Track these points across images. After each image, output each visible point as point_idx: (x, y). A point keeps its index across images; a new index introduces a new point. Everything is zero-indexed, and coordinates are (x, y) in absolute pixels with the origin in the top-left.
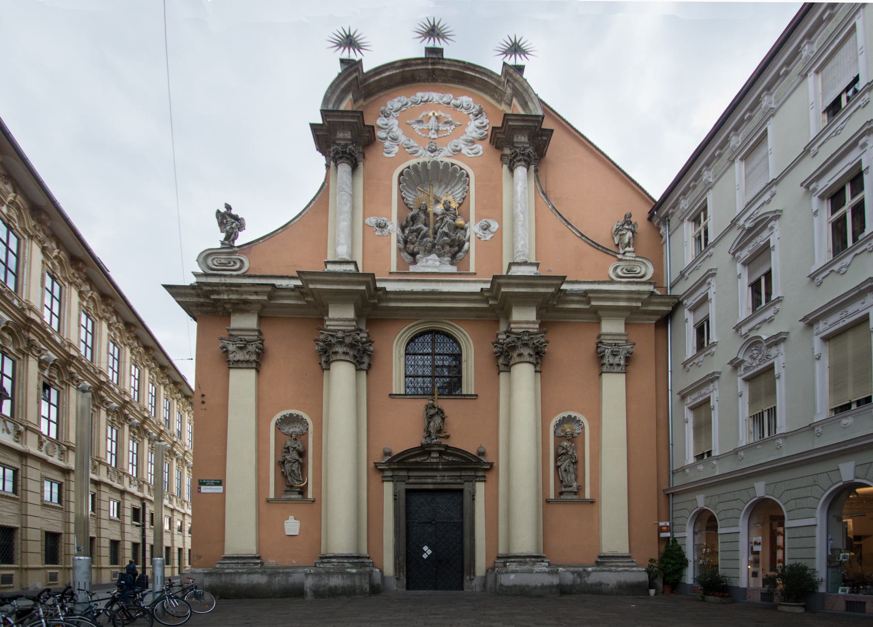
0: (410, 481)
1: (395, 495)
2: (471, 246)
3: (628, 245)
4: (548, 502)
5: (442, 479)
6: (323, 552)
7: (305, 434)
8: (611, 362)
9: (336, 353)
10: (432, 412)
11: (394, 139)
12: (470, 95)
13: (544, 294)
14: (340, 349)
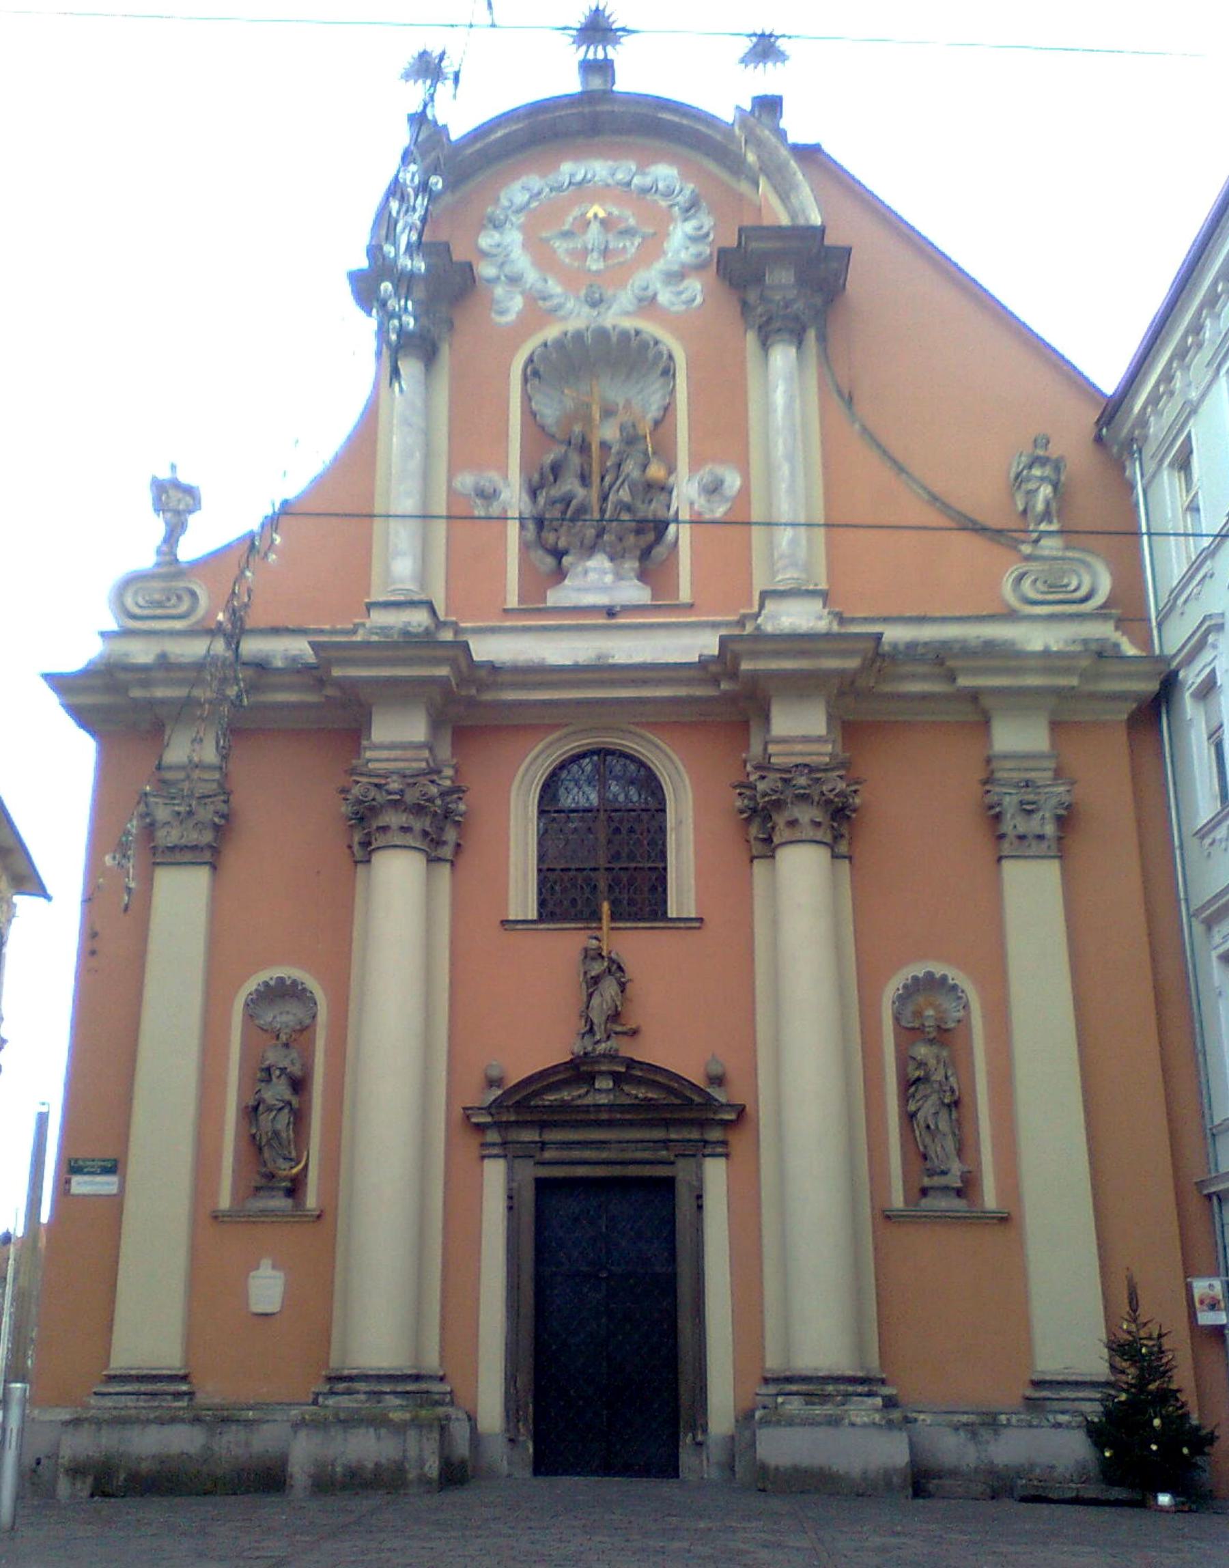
0: (548, 1155)
1: (510, 1198)
2: (682, 535)
3: (1047, 515)
4: (888, 1217)
5: (624, 1150)
6: (334, 1361)
7: (305, 1029)
8: (1021, 830)
9: (384, 829)
10: (597, 968)
11: (514, 280)
12: (673, 159)
13: (841, 673)
14: (393, 819)
